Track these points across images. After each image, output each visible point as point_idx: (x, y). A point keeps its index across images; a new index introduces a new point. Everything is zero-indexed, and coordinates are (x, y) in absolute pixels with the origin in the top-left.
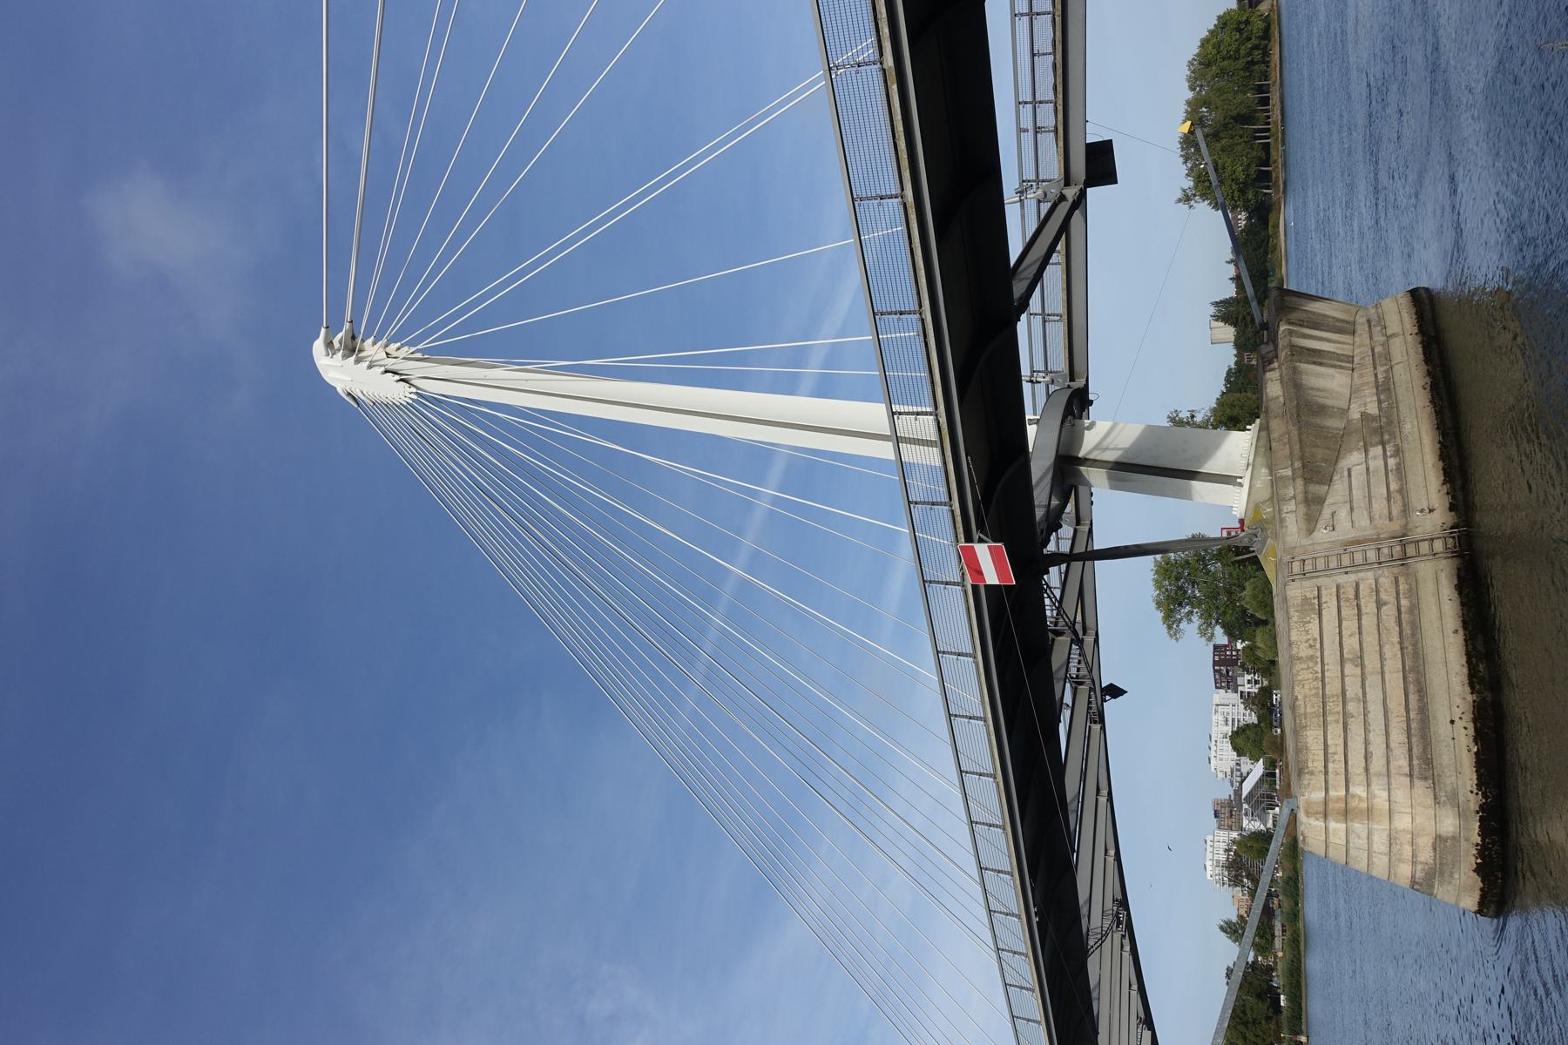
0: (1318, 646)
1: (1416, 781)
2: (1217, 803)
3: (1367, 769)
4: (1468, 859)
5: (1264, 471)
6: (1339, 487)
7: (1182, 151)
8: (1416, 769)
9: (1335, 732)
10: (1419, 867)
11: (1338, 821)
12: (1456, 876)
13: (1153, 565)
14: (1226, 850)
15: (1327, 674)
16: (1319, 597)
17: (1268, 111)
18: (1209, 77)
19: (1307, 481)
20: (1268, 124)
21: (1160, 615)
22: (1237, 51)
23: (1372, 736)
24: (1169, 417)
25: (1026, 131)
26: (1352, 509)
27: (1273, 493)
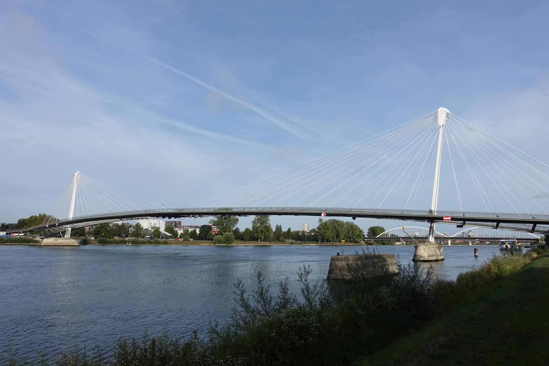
17: (338, 242)
20: (335, 242)
22: (354, 235)
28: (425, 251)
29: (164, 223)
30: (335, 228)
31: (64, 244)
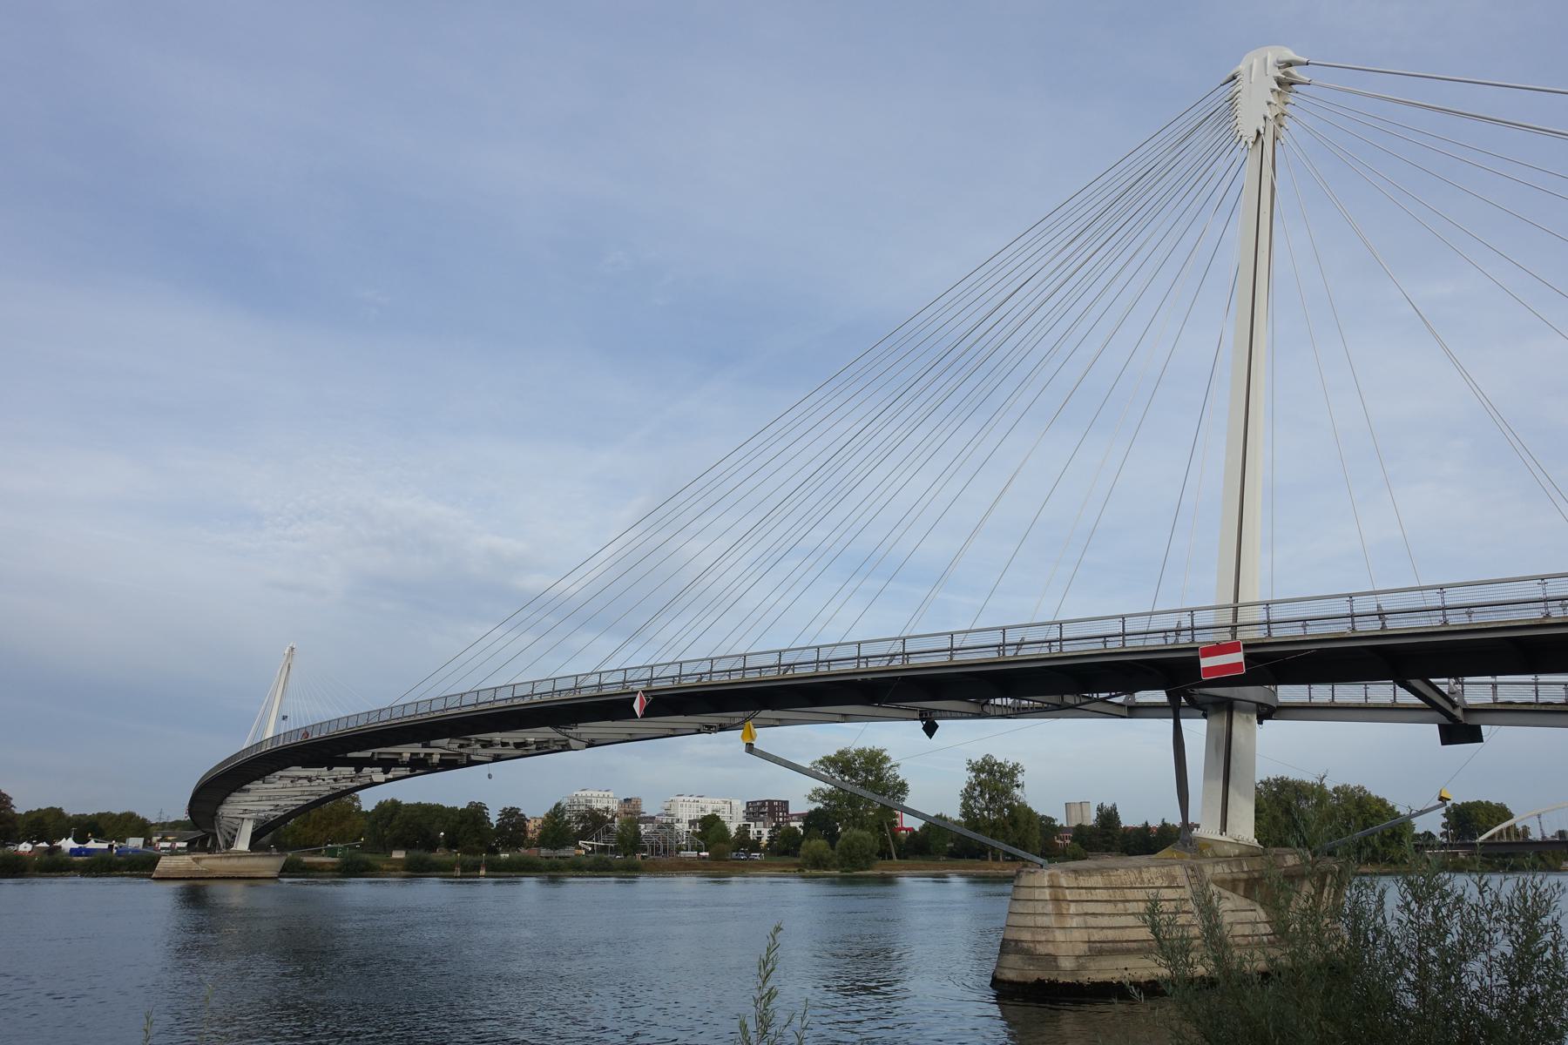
0: (1150, 885)
1: (1088, 944)
2: (638, 801)
3: (1086, 914)
4: (1046, 976)
5: (1237, 851)
6: (1244, 903)
7: (1274, 779)
8: (1094, 945)
9: (1101, 894)
10: (1031, 945)
11: (1050, 895)
12: (1031, 968)
13: (879, 748)
14: (607, 808)
15: (1136, 890)
16: (1179, 887)
18: (1345, 805)
19: (1246, 881)
21: (832, 753)
23: (1106, 918)
24: (1018, 764)
26: (1233, 911)
27: (1221, 857)
28: (1060, 915)
30: (1287, 811)
31: (226, 874)
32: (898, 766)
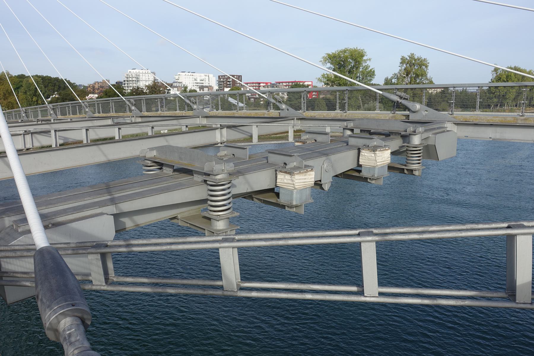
25: (408, 116)
29: (215, 78)
32: (370, 60)
